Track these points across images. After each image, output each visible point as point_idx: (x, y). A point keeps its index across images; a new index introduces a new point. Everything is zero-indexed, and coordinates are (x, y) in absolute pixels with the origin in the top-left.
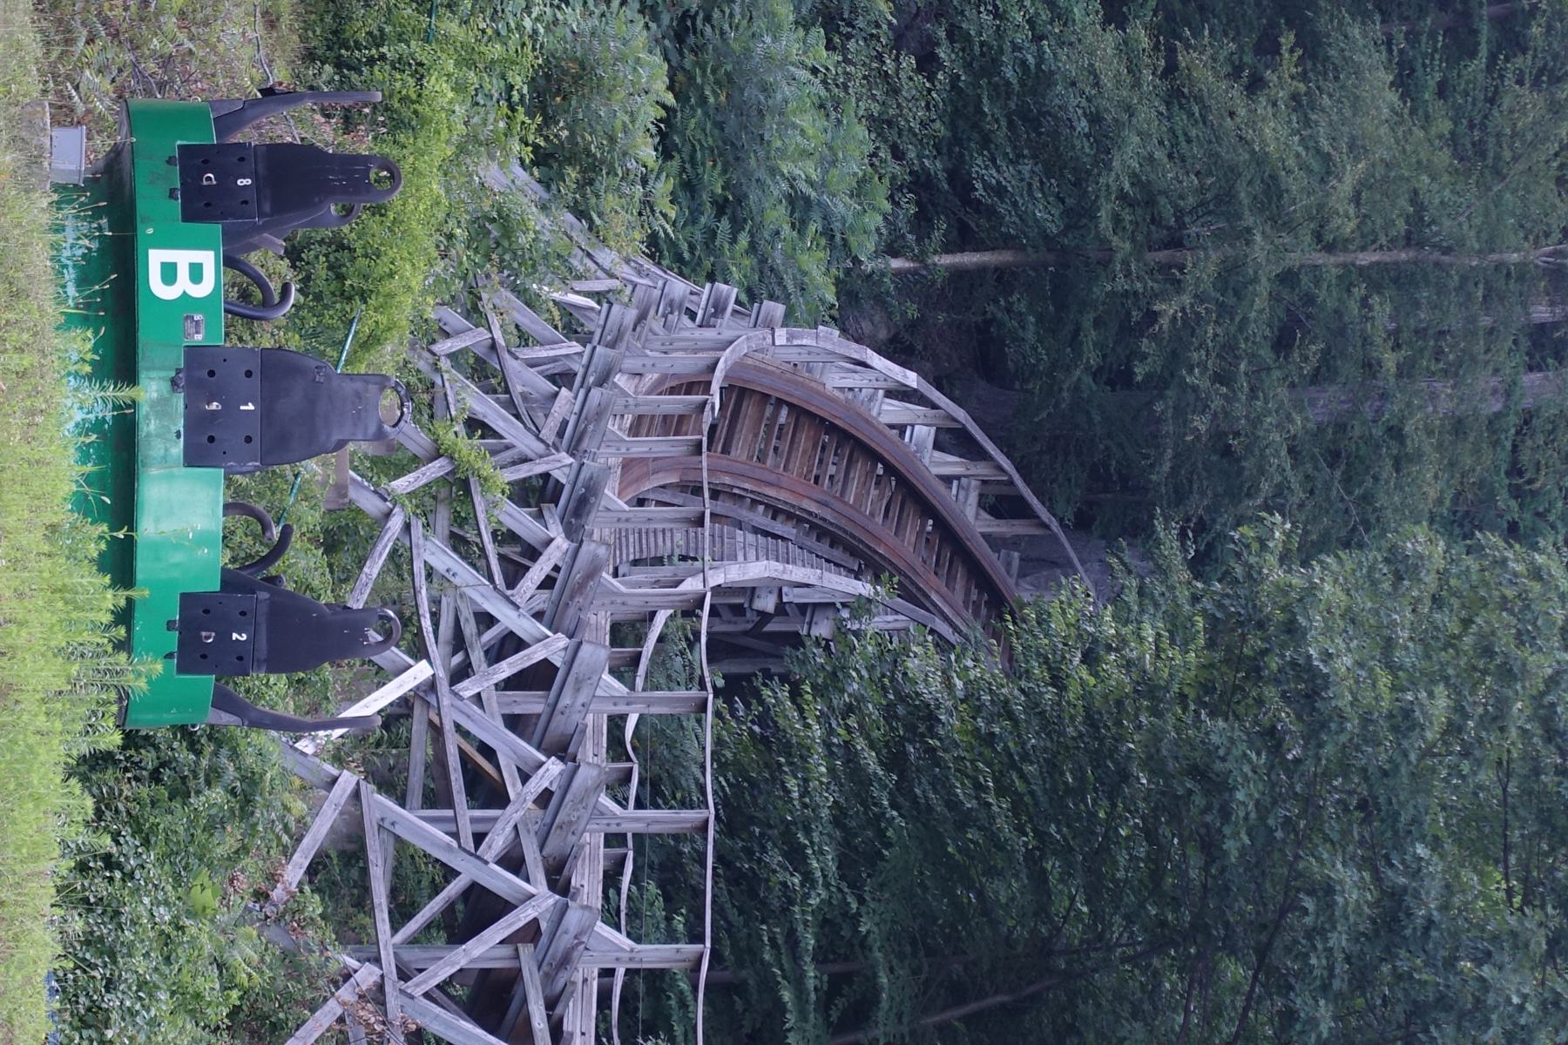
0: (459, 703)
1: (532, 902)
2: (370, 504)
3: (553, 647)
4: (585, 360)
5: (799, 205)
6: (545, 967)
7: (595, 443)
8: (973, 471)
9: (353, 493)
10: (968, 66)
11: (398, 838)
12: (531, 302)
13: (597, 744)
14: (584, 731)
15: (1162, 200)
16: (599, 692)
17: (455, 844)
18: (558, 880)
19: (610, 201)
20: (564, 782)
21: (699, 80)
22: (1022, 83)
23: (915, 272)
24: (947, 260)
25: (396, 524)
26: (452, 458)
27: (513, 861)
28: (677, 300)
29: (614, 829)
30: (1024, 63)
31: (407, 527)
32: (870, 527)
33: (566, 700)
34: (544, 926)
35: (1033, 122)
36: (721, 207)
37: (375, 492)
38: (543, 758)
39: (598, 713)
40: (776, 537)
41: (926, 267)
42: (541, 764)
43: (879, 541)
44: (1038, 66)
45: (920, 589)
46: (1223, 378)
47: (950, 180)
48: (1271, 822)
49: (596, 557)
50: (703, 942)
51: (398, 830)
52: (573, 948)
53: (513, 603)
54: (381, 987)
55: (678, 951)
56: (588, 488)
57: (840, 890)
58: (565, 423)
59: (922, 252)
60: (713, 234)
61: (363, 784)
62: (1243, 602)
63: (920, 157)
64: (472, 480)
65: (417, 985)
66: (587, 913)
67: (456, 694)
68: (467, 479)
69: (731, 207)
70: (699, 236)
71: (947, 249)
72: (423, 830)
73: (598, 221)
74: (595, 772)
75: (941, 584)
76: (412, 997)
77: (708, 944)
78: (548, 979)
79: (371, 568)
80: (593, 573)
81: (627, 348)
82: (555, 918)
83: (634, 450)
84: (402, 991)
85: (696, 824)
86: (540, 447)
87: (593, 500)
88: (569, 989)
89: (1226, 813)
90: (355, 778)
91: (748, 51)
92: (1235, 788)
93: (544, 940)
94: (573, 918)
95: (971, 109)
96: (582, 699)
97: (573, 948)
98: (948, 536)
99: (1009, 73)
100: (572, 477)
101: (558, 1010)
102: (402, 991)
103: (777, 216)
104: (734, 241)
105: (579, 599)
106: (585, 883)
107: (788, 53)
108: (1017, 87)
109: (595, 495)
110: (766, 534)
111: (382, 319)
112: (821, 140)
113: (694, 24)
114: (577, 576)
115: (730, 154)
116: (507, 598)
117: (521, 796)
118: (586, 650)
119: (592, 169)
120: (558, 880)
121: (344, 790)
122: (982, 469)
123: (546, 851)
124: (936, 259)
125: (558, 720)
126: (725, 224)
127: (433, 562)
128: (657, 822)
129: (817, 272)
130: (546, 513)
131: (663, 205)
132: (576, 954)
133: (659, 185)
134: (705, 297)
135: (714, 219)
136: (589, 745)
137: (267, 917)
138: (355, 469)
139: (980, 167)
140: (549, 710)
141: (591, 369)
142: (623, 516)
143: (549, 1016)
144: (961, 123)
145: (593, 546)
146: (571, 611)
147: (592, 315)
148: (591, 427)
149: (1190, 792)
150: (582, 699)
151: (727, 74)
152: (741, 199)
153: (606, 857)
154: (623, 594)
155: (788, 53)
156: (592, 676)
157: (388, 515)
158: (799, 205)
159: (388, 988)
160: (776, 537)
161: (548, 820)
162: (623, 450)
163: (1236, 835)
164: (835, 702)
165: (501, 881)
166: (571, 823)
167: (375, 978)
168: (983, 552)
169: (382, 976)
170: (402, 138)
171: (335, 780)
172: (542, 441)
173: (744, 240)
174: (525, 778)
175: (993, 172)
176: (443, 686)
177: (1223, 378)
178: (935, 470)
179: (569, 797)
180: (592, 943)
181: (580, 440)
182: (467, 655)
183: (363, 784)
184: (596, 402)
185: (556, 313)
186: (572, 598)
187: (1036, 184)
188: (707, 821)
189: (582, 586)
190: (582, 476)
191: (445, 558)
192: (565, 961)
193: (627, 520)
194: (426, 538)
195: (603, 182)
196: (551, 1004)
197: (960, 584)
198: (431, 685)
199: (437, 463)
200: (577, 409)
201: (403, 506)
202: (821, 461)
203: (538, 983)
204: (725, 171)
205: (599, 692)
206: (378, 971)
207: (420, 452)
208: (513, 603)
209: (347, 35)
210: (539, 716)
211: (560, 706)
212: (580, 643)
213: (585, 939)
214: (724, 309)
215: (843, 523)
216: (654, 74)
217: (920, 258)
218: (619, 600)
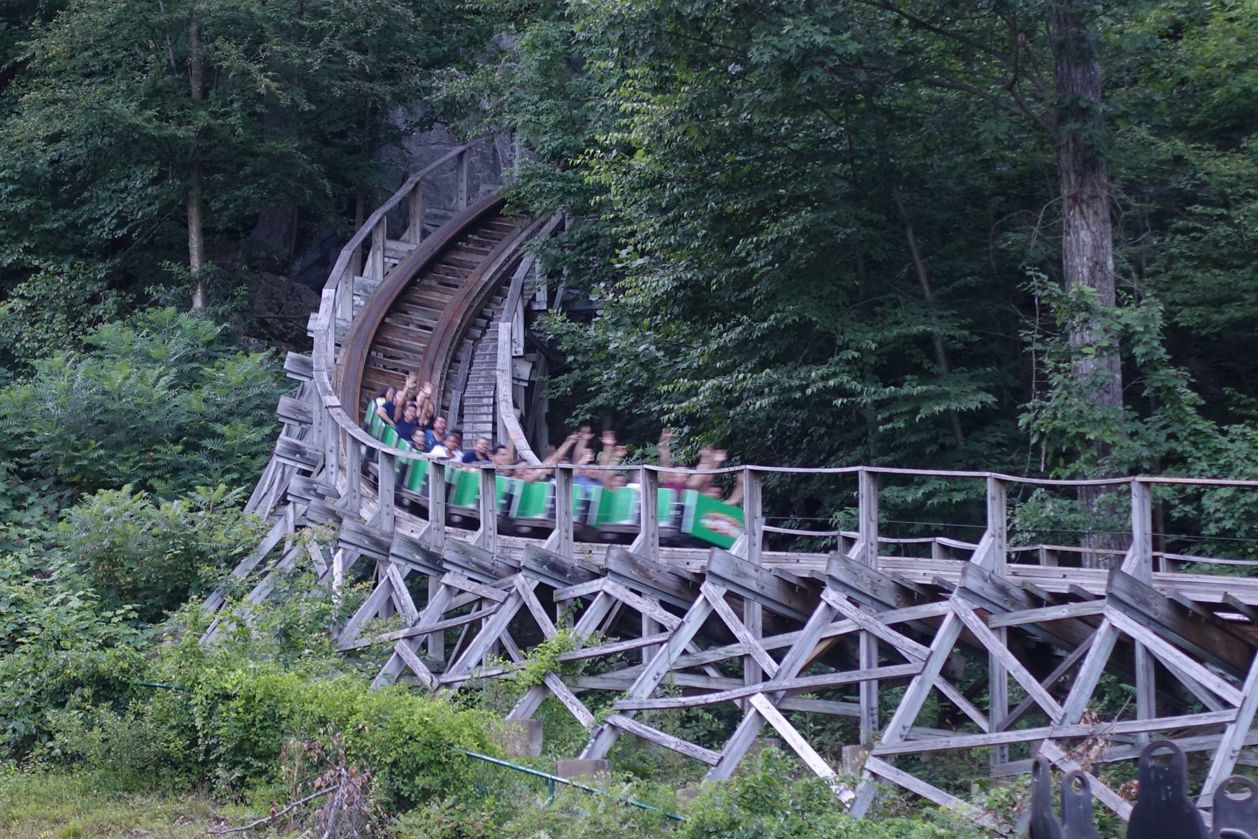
0: (783, 673)
1: (962, 615)
2: (606, 742)
3: (525, 584)
4: (402, 562)
5: (188, 381)
6: (1007, 606)
7: (488, 557)
8: (380, 244)
9: (598, 756)
10: (17, 240)
11: (915, 724)
12: (350, 608)
13: (788, 561)
14: (781, 571)
15: (160, 83)
16: (746, 558)
17: (918, 678)
18: (936, 592)
19: (221, 537)
20: (720, 582)
21: (85, 462)
22: (30, 195)
23: (206, 288)
24: (195, 261)
25: (624, 722)
26: (545, 674)
27: (924, 632)
28: (305, 485)
29: (875, 548)
30: (12, 194)
31: (623, 712)
32: (441, 329)
33: (753, 585)
34: (976, 606)
35: (59, 187)
36: (191, 447)
37: (596, 738)
38: (822, 605)
39: (761, 559)
40: (461, 407)
41: (201, 279)
42: (829, 606)
43: (450, 323)
44: (13, 181)
45: (482, 290)
46: (316, 37)
47: (114, 256)
48: (830, 14)
49: (618, 558)
50: (856, 473)
51: (910, 722)
52: (994, 583)
53: (679, 627)
54: (1058, 740)
55: (993, 498)
56: (543, 563)
57: (837, 364)
58: (849, 599)
59: (189, 281)
60: (213, 454)
61: (875, 752)
62: (641, 32)
63: (95, 280)
64: (563, 658)
65: (1054, 711)
66: (969, 572)
67: (777, 675)
68: (562, 662)
69: (192, 436)
70: (217, 465)
71: (187, 264)
72: (912, 700)
73: (239, 549)
74: (835, 562)
75: (473, 275)
76: (1065, 715)
77: (987, 474)
78: (1016, 604)
79: (669, 742)
80: (630, 560)
81: (374, 527)
82: (971, 597)
83: (491, 525)
84: (1061, 722)
85: (870, 481)
86: (511, 601)
87: (552, 559)
88: (1029, 588)
89: (827, 51)
90: (871, 758)
91: (59, 422)
92: (812, 43)
93: (987, 606)
94: (973, 583)
95: (50, 238)
96: (752, 572)
97: (994, 583)
98: (436, 265)
99: (22, 206)
100: (534, 576)
101: (1044, 596)
102: (1061, 722)
103: (192, 401)
104: (222, 436)
105: (652, 572)
106: (922, 572)
107: (60, 384)
108: (33, 200)
109: (549, 557)
110: (461, 415)
111: (467, 731)
112: (131, 364)
113: (25, 465)
114: (633, 573)
115: (145, 438)
116: (676, 631)
117: (854, 619)
118: (715, 568)
119: (193, 555)
120: (936, 592)
121: (884, 768)
122: (379, 238)
123: (894, 605)
124: (194, 270)
125: (768, 592)
126: (207, 443)
127: (648, 691)
128: (869, 513)
129: (245, 367)
130: (562, 598)
131: (216, 495)
132: (998, 581)
133: (199, 498)
134: (286, 462)
135: (201, 451)
136: (786, 566)
137: (1011, 832)
138: (578, 753)
139: (104, 231)
140: (759, 599)
141: (409, 557)
142: (564, 534)
143: (1049, 604)
144: (61, 246)
145: (610, 560)
146: (660, 579)
147: (348, 555)
148: (474, 559)
149: (811, 80)
150: (752, 572)
151: (78, 439)
152: (180, 429)
153: (1049, 564)
154: (646, 537)
155: (60, 384)
156: (734, 561)
157: (614, 727)
158: (188, 381)
159: (1060, 734)
160: (461, 407)
161: (868, 601)
162: (491, 533)
163: (843, 43)
164: (665, 364)
165: (944, 640)
166: (872, 583)
167: (1052, 744)
168: (438, 237)
169: (1050, 739)
170: (286, 712)
171: (874, 775)
172: (506, 600)
173: (219, 428)
174: (839, 617)
175: (107, 220)
176: (771, 685)
177: (316, 37)
178: (380, 276)
179: (853, 584)
180: (989, 567)
181: (484, 568)
182: (708, 664)
183: (875, 752)
184: (454, 554)
185: (359, 586)
186: (650, 578)
187: (113, 186)
188: (869, 473)
189: (641, 570)
190: (534, 568)
191: (645, 682)
192: (1003, 590)
193: (567, 531)
194: (631, 697)
195: (204, 546)
196: (1036, 601)
197: (463, 257)
198: (771, 695)
199: (552, 686)
200: (459, 570)
201: (607, 715)
202: (395, 370)
203: (1019, 613)
204: (161, 442)
205: (746, 558)
206: (1046, 742)
207: (538, 701)
208: (679, 627)
209: (180, 755)
210: (764, 608)
211: (757, 589)
212: (830, 576)
213: (987, 574)
214: (297, 446)
215: (444, 351)
216: (101, 501)
217: (193, 282)
218: (651, 539)
